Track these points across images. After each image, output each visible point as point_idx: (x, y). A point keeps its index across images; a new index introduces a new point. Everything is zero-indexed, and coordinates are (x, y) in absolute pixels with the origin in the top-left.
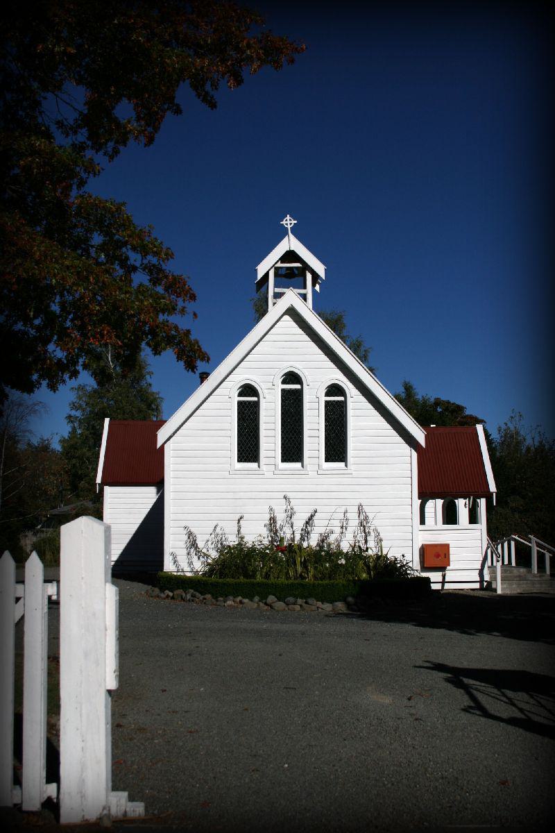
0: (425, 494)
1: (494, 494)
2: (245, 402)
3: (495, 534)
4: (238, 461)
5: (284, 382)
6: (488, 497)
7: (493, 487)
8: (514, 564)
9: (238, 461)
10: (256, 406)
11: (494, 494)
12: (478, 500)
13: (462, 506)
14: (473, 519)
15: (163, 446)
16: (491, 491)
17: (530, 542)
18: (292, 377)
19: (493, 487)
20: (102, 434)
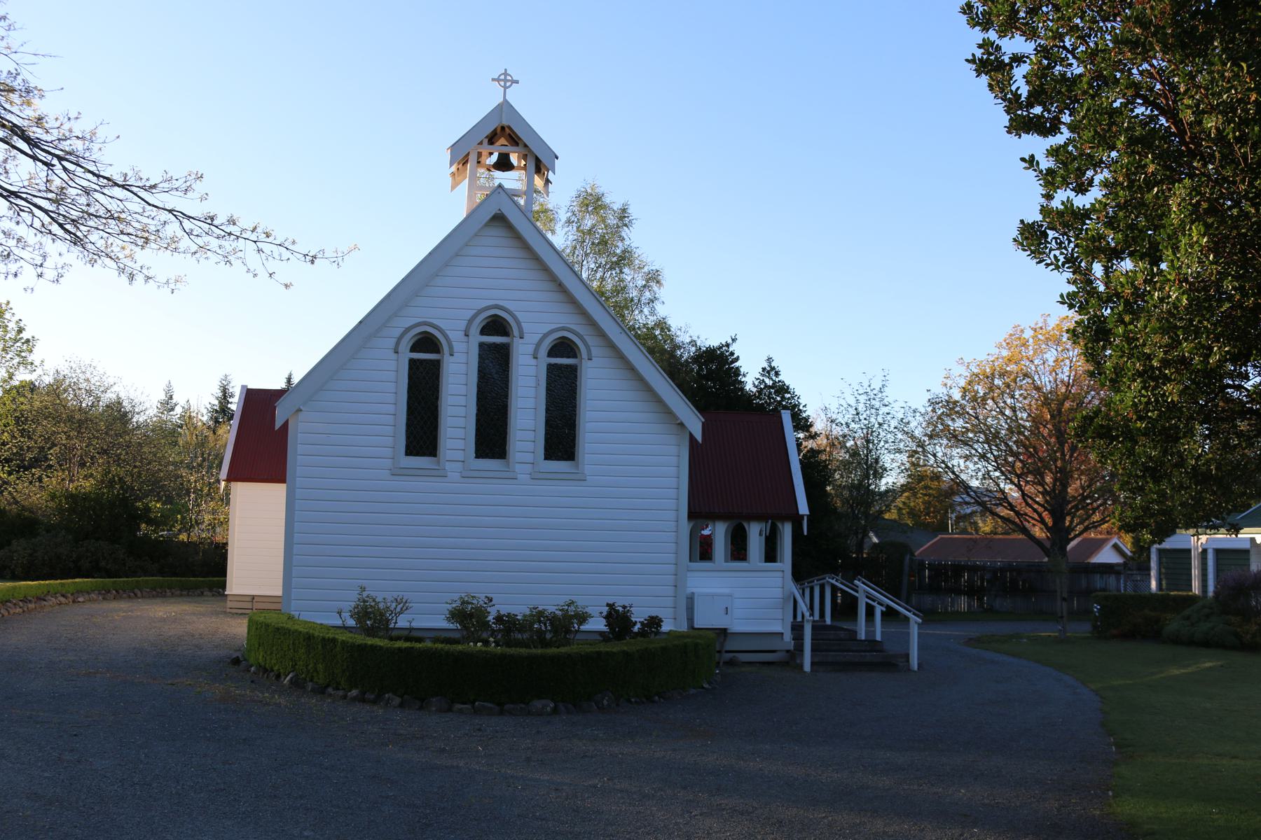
0: (699, 512)
1: (805, 518)
2: (422, 361)
3: (799, 574)
4: (546, 458)
5: (413, 349)
6: (796, 519)
7: (803, 508)
8: (828, 620)
9: (546, 458)
10: (435, 367)
11: (805, 518)
12: (779, 525)
13: (755, 535)
14: (771, 555)
15: (286, 424)
16: (801, 513)
17: (857, 592)
18: (496, 325)
19: (803, 508)
20: (562, 357)
